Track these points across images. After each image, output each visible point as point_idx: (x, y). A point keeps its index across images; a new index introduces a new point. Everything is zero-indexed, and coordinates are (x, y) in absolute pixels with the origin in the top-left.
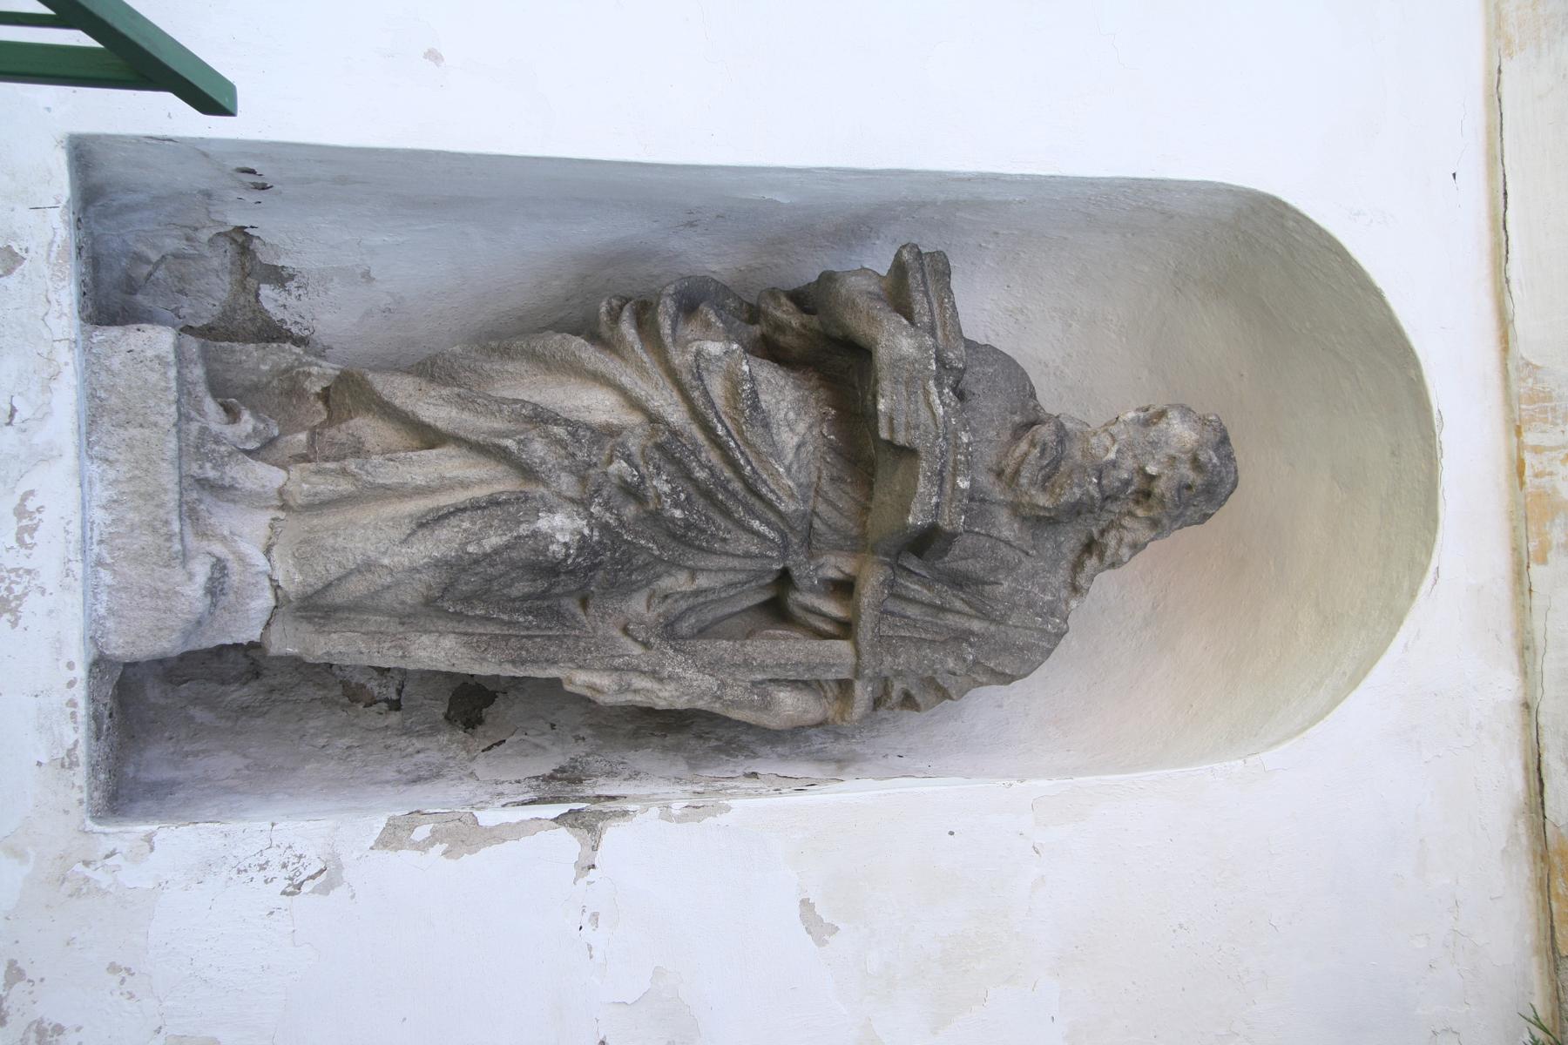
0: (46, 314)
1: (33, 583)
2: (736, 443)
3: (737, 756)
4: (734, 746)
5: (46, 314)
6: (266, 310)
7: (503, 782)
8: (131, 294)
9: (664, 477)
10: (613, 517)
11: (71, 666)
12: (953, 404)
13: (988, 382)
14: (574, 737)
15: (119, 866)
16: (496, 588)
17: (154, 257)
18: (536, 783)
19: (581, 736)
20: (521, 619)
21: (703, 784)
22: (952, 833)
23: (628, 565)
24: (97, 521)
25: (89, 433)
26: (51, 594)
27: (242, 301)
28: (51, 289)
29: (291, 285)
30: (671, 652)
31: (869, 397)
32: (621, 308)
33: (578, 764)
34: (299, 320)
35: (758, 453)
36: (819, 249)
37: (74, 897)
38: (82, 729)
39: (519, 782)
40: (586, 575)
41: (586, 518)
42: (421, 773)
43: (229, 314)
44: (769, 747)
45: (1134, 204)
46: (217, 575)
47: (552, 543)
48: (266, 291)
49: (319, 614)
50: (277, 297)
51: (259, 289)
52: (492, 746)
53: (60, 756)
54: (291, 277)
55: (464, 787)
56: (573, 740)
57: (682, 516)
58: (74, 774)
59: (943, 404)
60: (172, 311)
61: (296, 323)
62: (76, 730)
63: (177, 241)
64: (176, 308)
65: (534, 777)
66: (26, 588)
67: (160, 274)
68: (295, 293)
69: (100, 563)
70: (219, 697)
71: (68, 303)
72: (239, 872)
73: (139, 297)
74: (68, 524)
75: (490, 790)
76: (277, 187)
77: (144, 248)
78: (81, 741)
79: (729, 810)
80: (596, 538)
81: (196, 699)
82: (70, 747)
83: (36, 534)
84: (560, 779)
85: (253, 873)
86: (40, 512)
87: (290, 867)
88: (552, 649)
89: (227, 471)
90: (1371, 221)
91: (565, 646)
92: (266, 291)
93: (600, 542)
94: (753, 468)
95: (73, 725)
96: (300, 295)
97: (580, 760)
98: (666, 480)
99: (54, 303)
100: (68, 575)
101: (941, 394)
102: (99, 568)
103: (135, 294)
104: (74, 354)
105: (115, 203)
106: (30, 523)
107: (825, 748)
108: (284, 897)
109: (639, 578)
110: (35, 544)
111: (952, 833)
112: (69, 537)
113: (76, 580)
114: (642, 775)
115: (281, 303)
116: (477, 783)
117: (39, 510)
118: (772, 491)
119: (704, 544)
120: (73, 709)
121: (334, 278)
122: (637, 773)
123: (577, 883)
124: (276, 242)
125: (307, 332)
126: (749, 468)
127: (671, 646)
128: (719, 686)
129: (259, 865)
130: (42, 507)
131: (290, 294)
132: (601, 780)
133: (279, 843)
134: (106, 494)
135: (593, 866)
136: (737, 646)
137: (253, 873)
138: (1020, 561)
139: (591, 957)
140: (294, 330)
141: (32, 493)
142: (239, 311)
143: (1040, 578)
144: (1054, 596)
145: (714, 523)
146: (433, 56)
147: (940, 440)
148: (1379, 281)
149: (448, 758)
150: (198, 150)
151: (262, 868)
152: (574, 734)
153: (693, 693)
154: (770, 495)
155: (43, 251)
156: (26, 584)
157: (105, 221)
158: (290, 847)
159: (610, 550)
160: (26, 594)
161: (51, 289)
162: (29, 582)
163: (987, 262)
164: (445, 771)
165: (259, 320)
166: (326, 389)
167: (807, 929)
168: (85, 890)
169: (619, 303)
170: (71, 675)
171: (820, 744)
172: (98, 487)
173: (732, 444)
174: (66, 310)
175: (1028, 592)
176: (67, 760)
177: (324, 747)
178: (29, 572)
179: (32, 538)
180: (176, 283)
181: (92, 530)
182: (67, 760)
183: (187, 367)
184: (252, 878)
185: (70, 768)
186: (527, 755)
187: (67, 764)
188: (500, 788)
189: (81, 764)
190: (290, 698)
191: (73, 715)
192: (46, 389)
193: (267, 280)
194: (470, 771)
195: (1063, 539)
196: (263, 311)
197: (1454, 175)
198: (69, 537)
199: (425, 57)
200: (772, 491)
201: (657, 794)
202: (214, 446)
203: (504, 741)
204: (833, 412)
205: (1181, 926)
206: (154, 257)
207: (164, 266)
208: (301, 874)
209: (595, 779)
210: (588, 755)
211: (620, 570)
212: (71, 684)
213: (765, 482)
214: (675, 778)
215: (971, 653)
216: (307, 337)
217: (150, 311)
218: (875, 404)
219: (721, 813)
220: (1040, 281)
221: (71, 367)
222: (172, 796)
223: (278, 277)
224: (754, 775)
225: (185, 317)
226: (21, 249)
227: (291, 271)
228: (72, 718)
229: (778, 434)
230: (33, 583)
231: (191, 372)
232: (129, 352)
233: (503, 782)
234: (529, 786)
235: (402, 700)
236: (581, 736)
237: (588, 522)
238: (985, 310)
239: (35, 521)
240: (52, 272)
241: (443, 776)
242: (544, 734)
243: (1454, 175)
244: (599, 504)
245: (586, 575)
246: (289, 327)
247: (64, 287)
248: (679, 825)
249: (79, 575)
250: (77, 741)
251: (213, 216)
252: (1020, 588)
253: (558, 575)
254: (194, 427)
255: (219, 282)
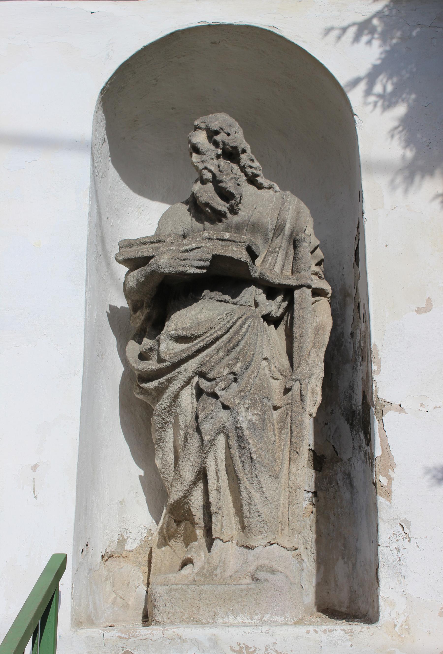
0: (151, 640)
1: (271, 647)
2: (207, 337)
3: (342, 342)
4: (337, 343)
5: (151, 640)
6: (136, 547)
7: (353, 446)
8: (129, 606)
9: (222, 370)
10: (240, 393)
11: (308, 632)
12: (190, 240)
13: (176, 224)
14: (331, 415)
15: (396, 612)
16: (271, 446)
17: (114, 595)
18: (354, 432)
19: (331, 411)
20: (284, 436)
21: (357, 357)
22: (387, 246)
23: (261, 387)
24: (242, 621)
25: (203, 623)
26: (276, 640)
27: (132, 558)
28: (140, 638)
29: (125, 536)
30: (299, 369)
31: (185, 277)
32: (140, 388)
33: (345, 413)
34: (140, 533)
35: (211, 328)
36: (111, 299)
37: (410, 631)
38: (337, 627)
39: (353, 439)
40: (265, 406)
41: (241, 406)
42: (348, 483)
43: (137, 564)
44: (338, 327)
45: (99, 155)
46: (265, 570)
47: (252, 421)
48: (128, 547)
49: (280, 525)
50: (130, 543)
51: (127, 550)
52: (335, 451)
53: (348, 637)
54: (122, 536)
55: (355, 464)
56: (333, 415)
57: (240, 363)
58: (356, 631)
59: (190, 244)
60: (136, 589)
61: (141, 534)
62: (336, 630)
63: (107, 586)
64: (135, 587)
65: (351, 433)
66: (273, 651)
67: (121, 593)
68: (128, 534)
69: (261, 619)
70: (309, 572)
71: (146, 630)
72: (400, 560)
73: (130, 603)
74: (245, 632)
75: (357, 452)
76: (87, 540)
77: (110, 600)
78: (341, 628)
79: (376, 344)
80: (250, 402)
81: (310, 581)
82: (344, 633)
83: (250, 646)
84: (353, 421)
85: (400, 554)
86: (240, 644)
87: (398, 538)
88: (297, 423)
89: (217, 564)
90: (112, 50)
91: (296, 417)
92: (128, 547)
93: (251, 400)
94: (219, 330)
95: (334, 631)
96: (130, 532)
97: (343, 412)
98: (224, 369)
99: (147, 636)
100: (268, 633)
101: (186, 245)
102: (263, 620)
103: (129, 605)
104: (169, 629)
105: (93, 611)
106: (244, 649)
107: (338, 302)
108: (411, 541)
109: (266, 383)
110: (254, 646)
111: (387, 246)
112: (251, 632)
113: (270, 629)
114: (351, 384)
115: (133, 541)
116: (353, 457)
117: (239, 645)
118: (228, 322)
119: (252, 353)
120: (327, 632)
121: (123, 517)
122: (350, 386)
123: (407, 412)
124: (108, 542)
125: (146, 530)
126: (218, 332)
127: (297, 369)
128: (314, 348)
129: (397, 552)
130: (237, 643)
131: (129, 537)
132: (353, 402)
133: (388, 543)
134: (230, 616)
135: (400, 405)
136: (296, 340)
137: (400, 554)
138: (259, 212)
139: (440, 407)
140: (145, 535)
141: (231, 648)
142: (136, 560)
143: (266, 203)
144: (274, 197)
145: (243, 349)
146: (34, 468)
147: (207, 245)
148: (139, 47)
149: (341, 471)
150: (77, 571)
151: (398, 550)
152: (330, 415)
153: (317, 360)
154: (231, 323)
155: (123, 641)
156: (271, 651)
157: (99, 616)
158: (389, 538)
159: (255, 395)
160: (276, 650)
161: (140, 638)
162: (271, 649)
163: (118, 223)
164: (347, 472)
165: (140, 550)
166: (175, 521)
167: (428, 311)
168: (407, 627)
169: (138, 389)
170: (312, 632)
171: (336, 304)
172: (226, 620)
173: (207, 339)
174: (150, 631)
175: (272, 209)
176: (350, 634)
177: (334, 526)
178: (266, 649)
179: (251, 648)
180: (125, 586)
181: (245, 623)
182: (350, 634)
183: (168, 581)
184: (403, 555)
185: (353, 633)
186: (340, 436)
187: (351, 634)
188: (357, 447)
189: (351, 628)
190: (310, 540)
191: (330, 631)
192: (185, 641)
193: (123, 547)
194: (347, 461)
195: (248, 192)
196: (136, 549)
197: (92, 13)
198: (251, 632)
199: (35, 471)
200: (228, 322)
201: (362, 377)
202: (205, 570)
203: (333, 446)
204: (191, 294)
205: (428, 146)
206: (114, 595)
207: (117, 592)
208: (401, 534)
209: (353, 405)
210: (341, 408)
211: (263, 391)
212: (316, 632)
213: (225, 325)
214: (353, 369)
215: (302, 235)
216: (148, 530)
217: (136, 598)
218: (190, 274)
219: (377, 348)
220: (127, 199)
221: (176, 630)
222: (357, 591)
223: (122, 541)
224: (352, 334)
225: (139, 583)
226: (122, 650)
227: (120, 536)
228: (331, 632)
229: (202, 318)
230: (271, 647)
231: (170, 580)
232: (165, 605)
233: (353, 446)
234: (356, 435)
235: (312, 491)
236: (331, 411)
237: (242, 405)
238: (138, 225)
239: (244, 646)
240: (133, 637)
241: (349, 473)
242: (330, 428)
243: (92, 13)
244: (234, 399)
245: (265, 406)
246: (143, 538)
247: (139, 632)
248: (382, 367)
249: (268, 628)
250: (341, 630)
251: (98, 569)
252: (270, 212)
253: (265, 419)
254: (198, 578)
255: (124, 568)
